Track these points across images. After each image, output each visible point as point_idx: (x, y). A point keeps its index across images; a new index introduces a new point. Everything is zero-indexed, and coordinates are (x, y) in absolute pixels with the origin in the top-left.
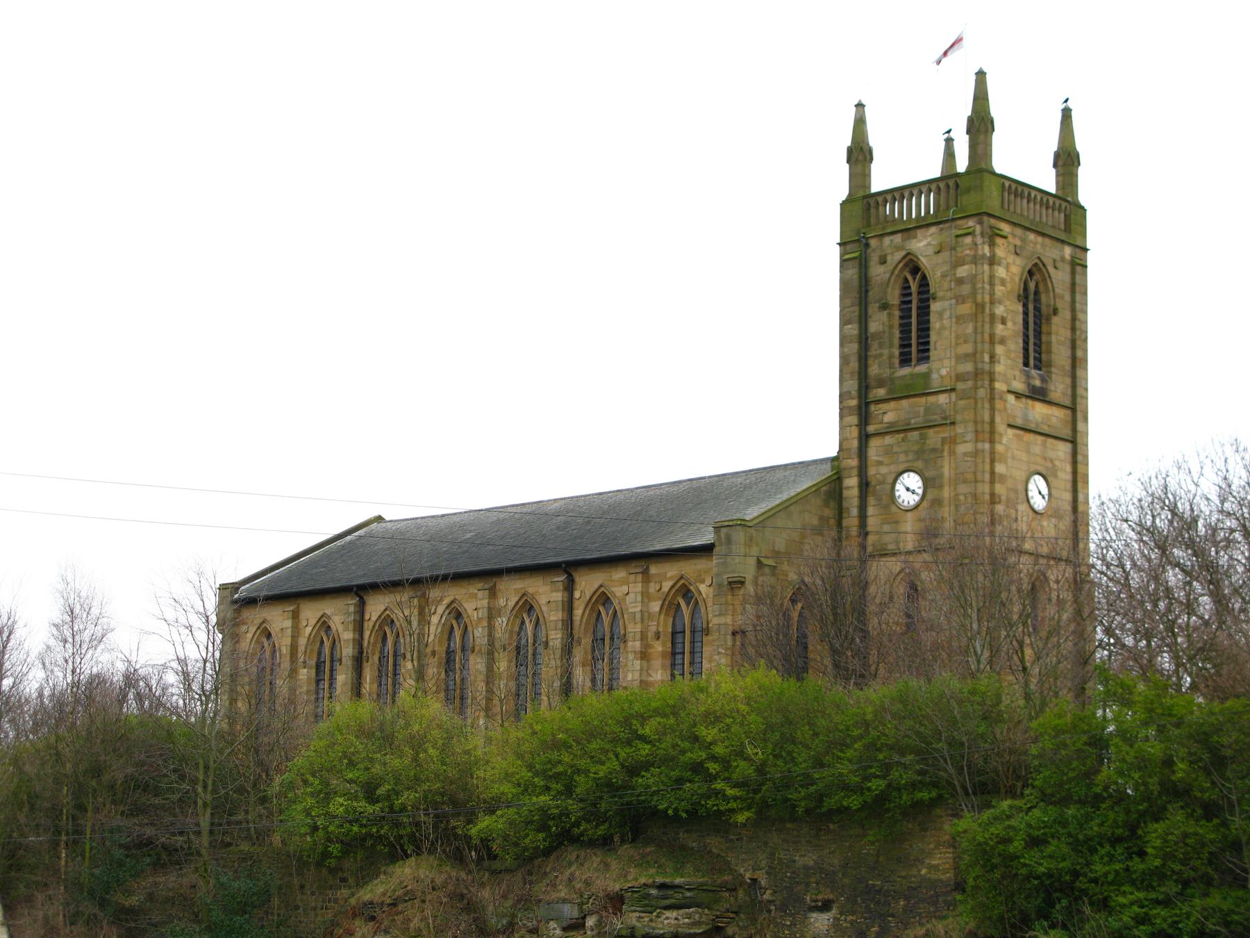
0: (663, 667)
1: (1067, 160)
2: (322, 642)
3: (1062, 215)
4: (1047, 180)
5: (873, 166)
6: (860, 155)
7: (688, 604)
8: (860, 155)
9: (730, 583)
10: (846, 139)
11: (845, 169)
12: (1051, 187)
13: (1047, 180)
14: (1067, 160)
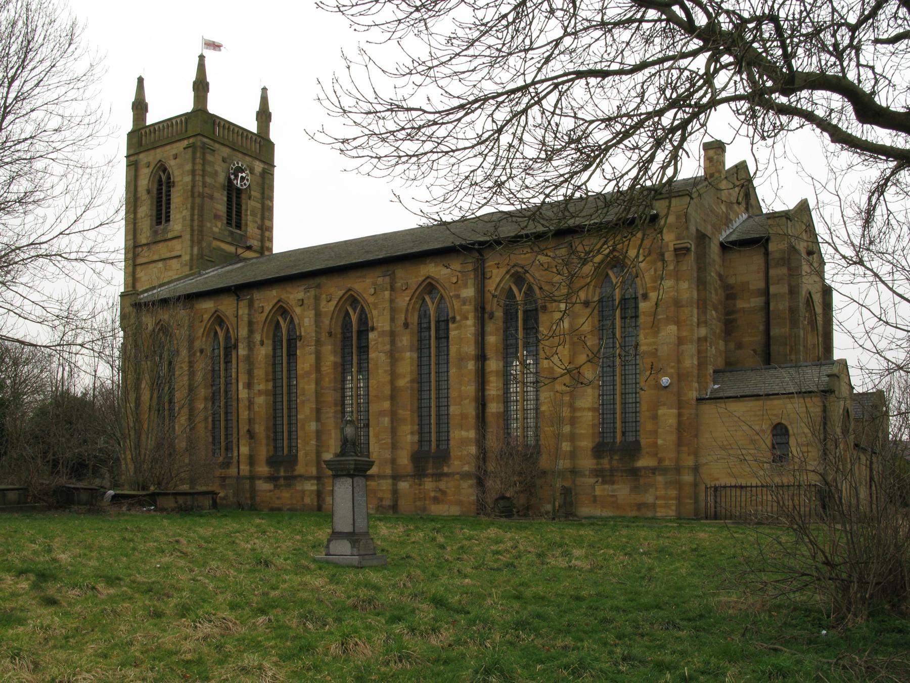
0: (334, 352)
1: (264, 116)
2: (216, 333)
3: (258, 146)
4: (252, 127)
5: (209, 95)
6: (140, 107)
7: (355, 310)
8: (140, 107)
9: (676, 250)
10: (193, 76)
11: (191, 94)
12: (255, 130)
13: (252, 127)
14: (264, 116)
